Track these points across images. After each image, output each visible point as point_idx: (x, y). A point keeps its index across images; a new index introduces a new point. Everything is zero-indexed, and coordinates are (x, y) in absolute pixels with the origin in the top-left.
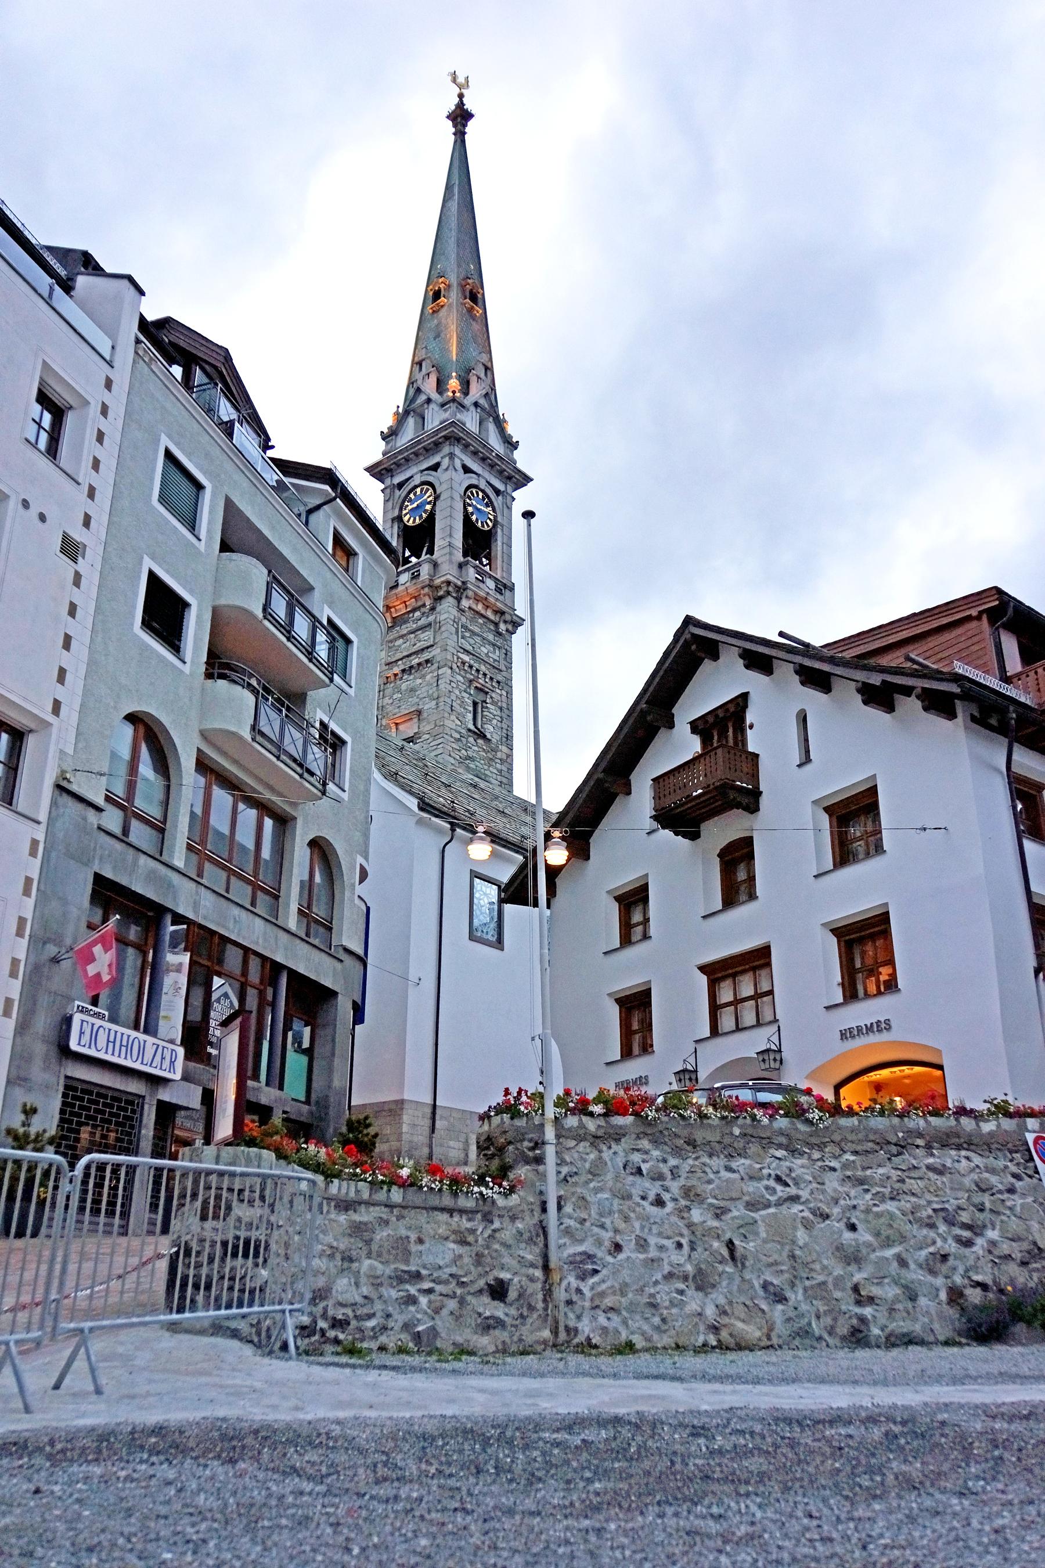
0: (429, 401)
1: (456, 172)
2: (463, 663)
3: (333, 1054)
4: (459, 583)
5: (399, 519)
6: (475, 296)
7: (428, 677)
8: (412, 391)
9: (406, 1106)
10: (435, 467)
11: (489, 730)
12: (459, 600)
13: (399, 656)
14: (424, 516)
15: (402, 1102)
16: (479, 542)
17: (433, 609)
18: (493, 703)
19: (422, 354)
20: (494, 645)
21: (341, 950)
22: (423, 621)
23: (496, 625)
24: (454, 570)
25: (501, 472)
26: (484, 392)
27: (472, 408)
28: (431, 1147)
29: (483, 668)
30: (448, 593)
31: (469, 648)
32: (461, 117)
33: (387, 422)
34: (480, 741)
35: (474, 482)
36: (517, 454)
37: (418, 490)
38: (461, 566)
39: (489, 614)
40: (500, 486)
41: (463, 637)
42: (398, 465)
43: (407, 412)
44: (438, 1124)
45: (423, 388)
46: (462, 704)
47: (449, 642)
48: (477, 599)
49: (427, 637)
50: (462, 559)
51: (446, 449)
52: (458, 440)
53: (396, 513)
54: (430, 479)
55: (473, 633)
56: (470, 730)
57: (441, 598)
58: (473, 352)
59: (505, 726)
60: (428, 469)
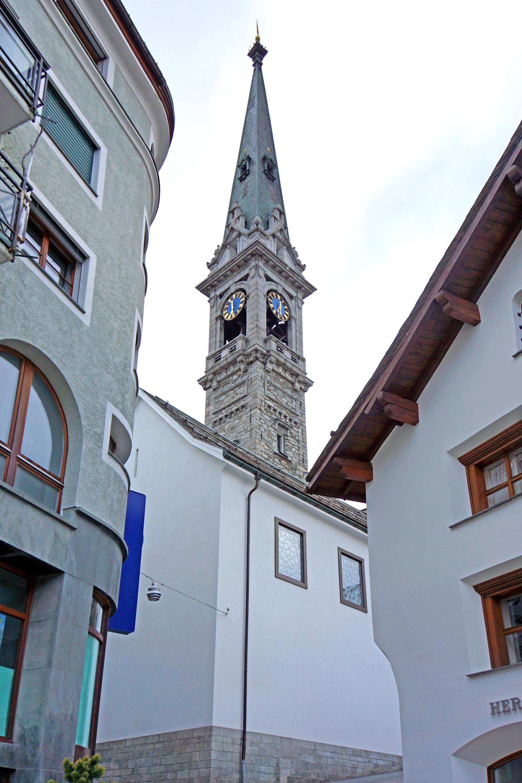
0: (240, 235)
1: (255, 88)
2: (269, 407)
3: (50, 664)
4: (265, 352)
5: (221, 317)
6: (271, 170)
7: (244, 418)
8: (228, 232)
9: (214, 733)
10: (245, 278)
11: (290, 454)
12: (265, 364)
13: (222, 406)
14: (238, 311)
15: (211, 728)
16: (280, 329)
17: (246, 371)
18: (292, 436)
19: (234, 205)
20: (292, 398)
21: (73, 514)
22: (240, 380)
23: (293, 384)
24: (261, 343)
25: (293, 283)
26: (280, 228)
27: (271, 238)
28: (241, 772)
29: (284, 412)
30: (257, 358)
31: (274, 398)
32: (258, 53)
33: (210, 256)
34: (283, 462)
35: (274, 287)
36: (304, 274)
37: (234, 296)
38: (265, 341)
39: (287, 375)
40: (294, 294)
41: (269, 390)
42: (219, 281)
43: (224, 246)
44: (248, 750)
45: (235, 227)
46: (269, 435)
47: (258, 392)
48: (278, 363)
49: (242, 391)
50: (266, 337)
51: (253, 263)
52: (261, 256)
53: (219, 313)
54: (242, 286)
55: (276, 388)
56: (275, 453)
57: (251, 363)
58: (271, 204)
59: (301, 453)
60: (240, 280)
